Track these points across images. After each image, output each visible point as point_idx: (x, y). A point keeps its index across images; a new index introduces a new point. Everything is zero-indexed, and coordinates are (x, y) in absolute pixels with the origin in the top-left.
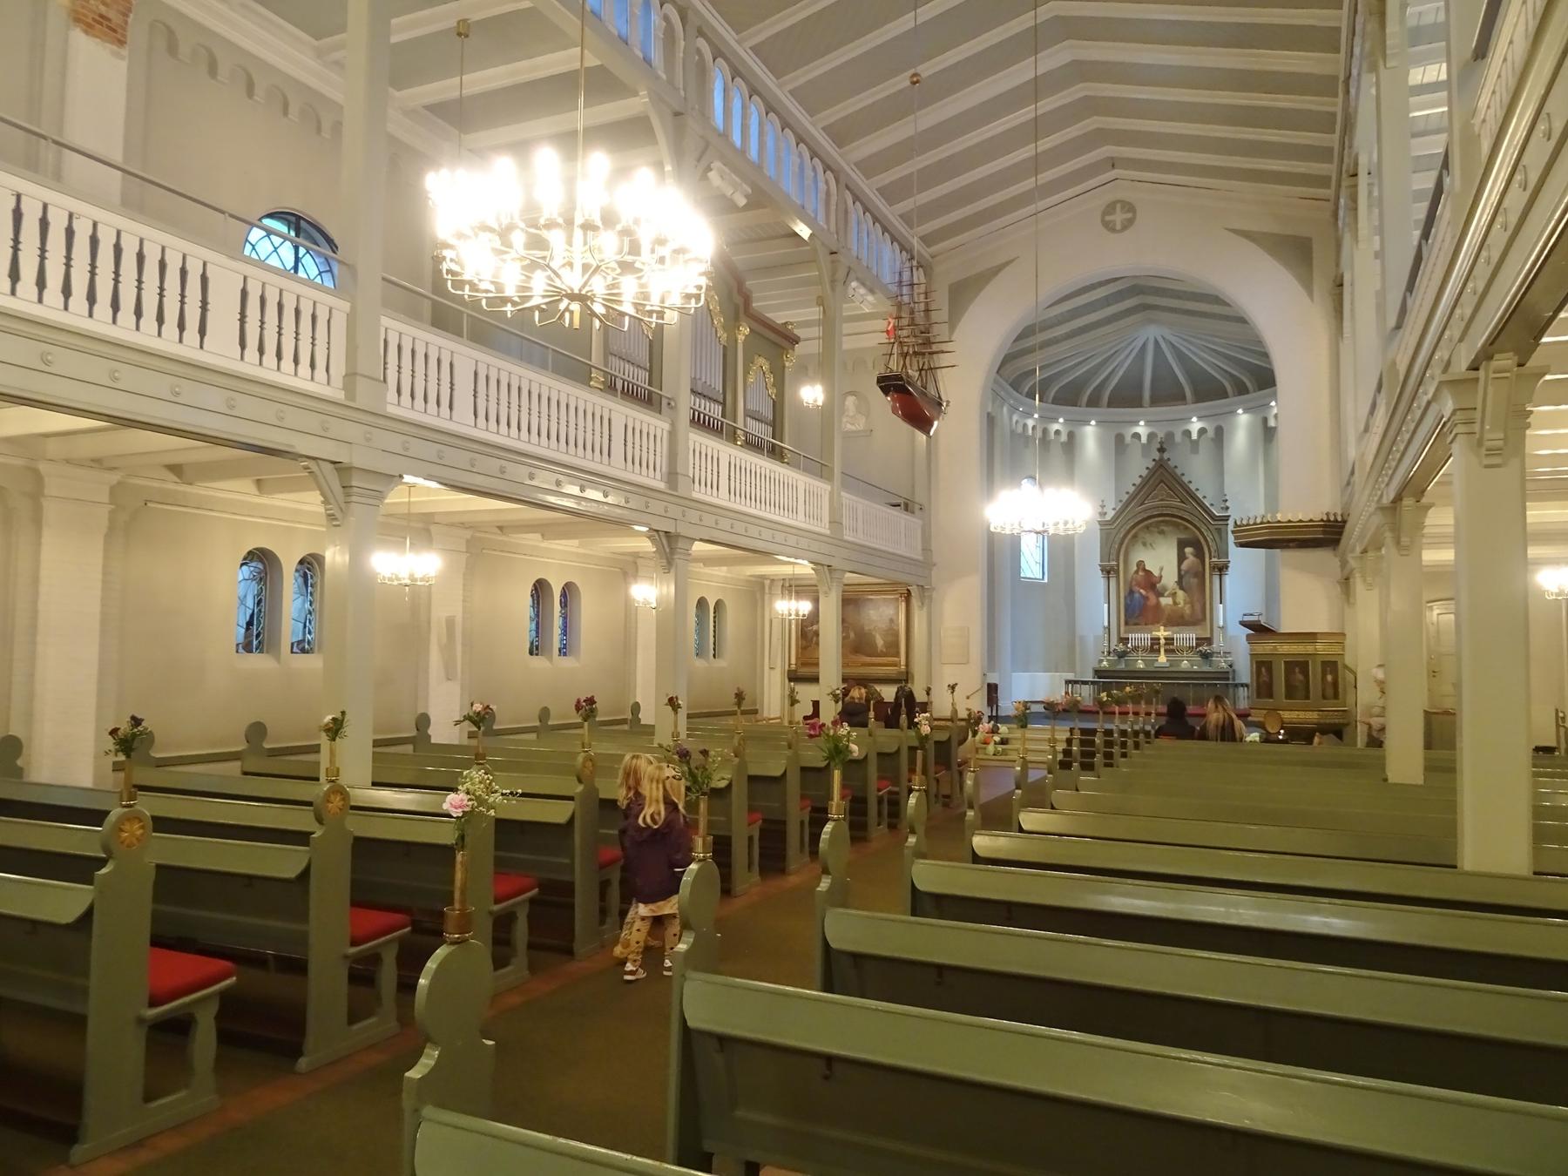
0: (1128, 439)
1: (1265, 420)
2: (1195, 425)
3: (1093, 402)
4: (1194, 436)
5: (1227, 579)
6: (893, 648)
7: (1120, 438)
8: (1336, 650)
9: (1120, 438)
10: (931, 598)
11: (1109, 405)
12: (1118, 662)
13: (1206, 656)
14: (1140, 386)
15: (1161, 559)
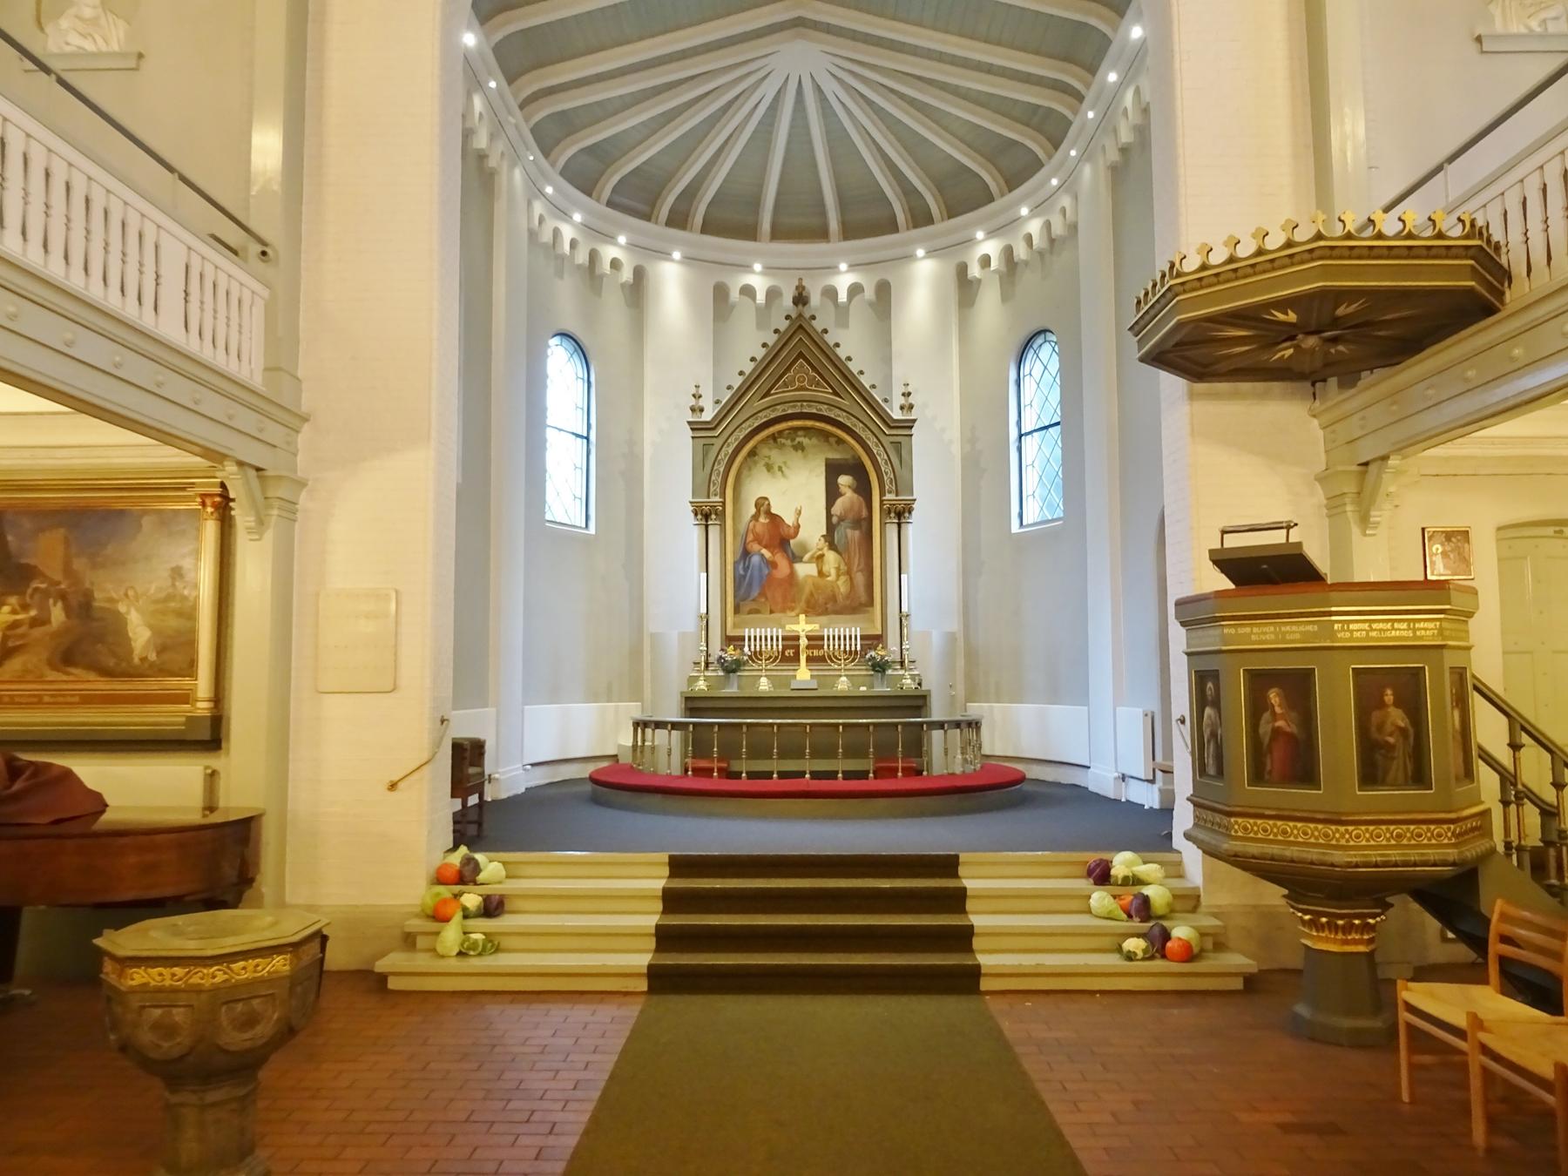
0: (735, 295)
1: (962, 269)
2: (844, 281)
3: (678, 220)
4: (843, 297)
5: (910, 531)
6: (175, 653)
7: (721, 292)
8: (1426, 629)
9: (721, 292)
10: (290, 507)
11: (705, 230)
12: (725, 681)
13: (880, 667)
14: (755, 204)
15: (796, 491)
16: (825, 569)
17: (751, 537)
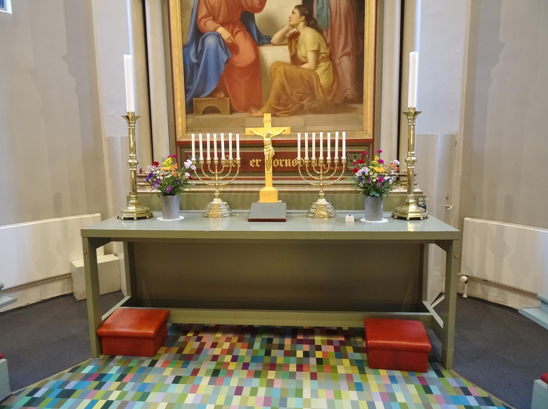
16: (301, 52)
17: (203, 11)
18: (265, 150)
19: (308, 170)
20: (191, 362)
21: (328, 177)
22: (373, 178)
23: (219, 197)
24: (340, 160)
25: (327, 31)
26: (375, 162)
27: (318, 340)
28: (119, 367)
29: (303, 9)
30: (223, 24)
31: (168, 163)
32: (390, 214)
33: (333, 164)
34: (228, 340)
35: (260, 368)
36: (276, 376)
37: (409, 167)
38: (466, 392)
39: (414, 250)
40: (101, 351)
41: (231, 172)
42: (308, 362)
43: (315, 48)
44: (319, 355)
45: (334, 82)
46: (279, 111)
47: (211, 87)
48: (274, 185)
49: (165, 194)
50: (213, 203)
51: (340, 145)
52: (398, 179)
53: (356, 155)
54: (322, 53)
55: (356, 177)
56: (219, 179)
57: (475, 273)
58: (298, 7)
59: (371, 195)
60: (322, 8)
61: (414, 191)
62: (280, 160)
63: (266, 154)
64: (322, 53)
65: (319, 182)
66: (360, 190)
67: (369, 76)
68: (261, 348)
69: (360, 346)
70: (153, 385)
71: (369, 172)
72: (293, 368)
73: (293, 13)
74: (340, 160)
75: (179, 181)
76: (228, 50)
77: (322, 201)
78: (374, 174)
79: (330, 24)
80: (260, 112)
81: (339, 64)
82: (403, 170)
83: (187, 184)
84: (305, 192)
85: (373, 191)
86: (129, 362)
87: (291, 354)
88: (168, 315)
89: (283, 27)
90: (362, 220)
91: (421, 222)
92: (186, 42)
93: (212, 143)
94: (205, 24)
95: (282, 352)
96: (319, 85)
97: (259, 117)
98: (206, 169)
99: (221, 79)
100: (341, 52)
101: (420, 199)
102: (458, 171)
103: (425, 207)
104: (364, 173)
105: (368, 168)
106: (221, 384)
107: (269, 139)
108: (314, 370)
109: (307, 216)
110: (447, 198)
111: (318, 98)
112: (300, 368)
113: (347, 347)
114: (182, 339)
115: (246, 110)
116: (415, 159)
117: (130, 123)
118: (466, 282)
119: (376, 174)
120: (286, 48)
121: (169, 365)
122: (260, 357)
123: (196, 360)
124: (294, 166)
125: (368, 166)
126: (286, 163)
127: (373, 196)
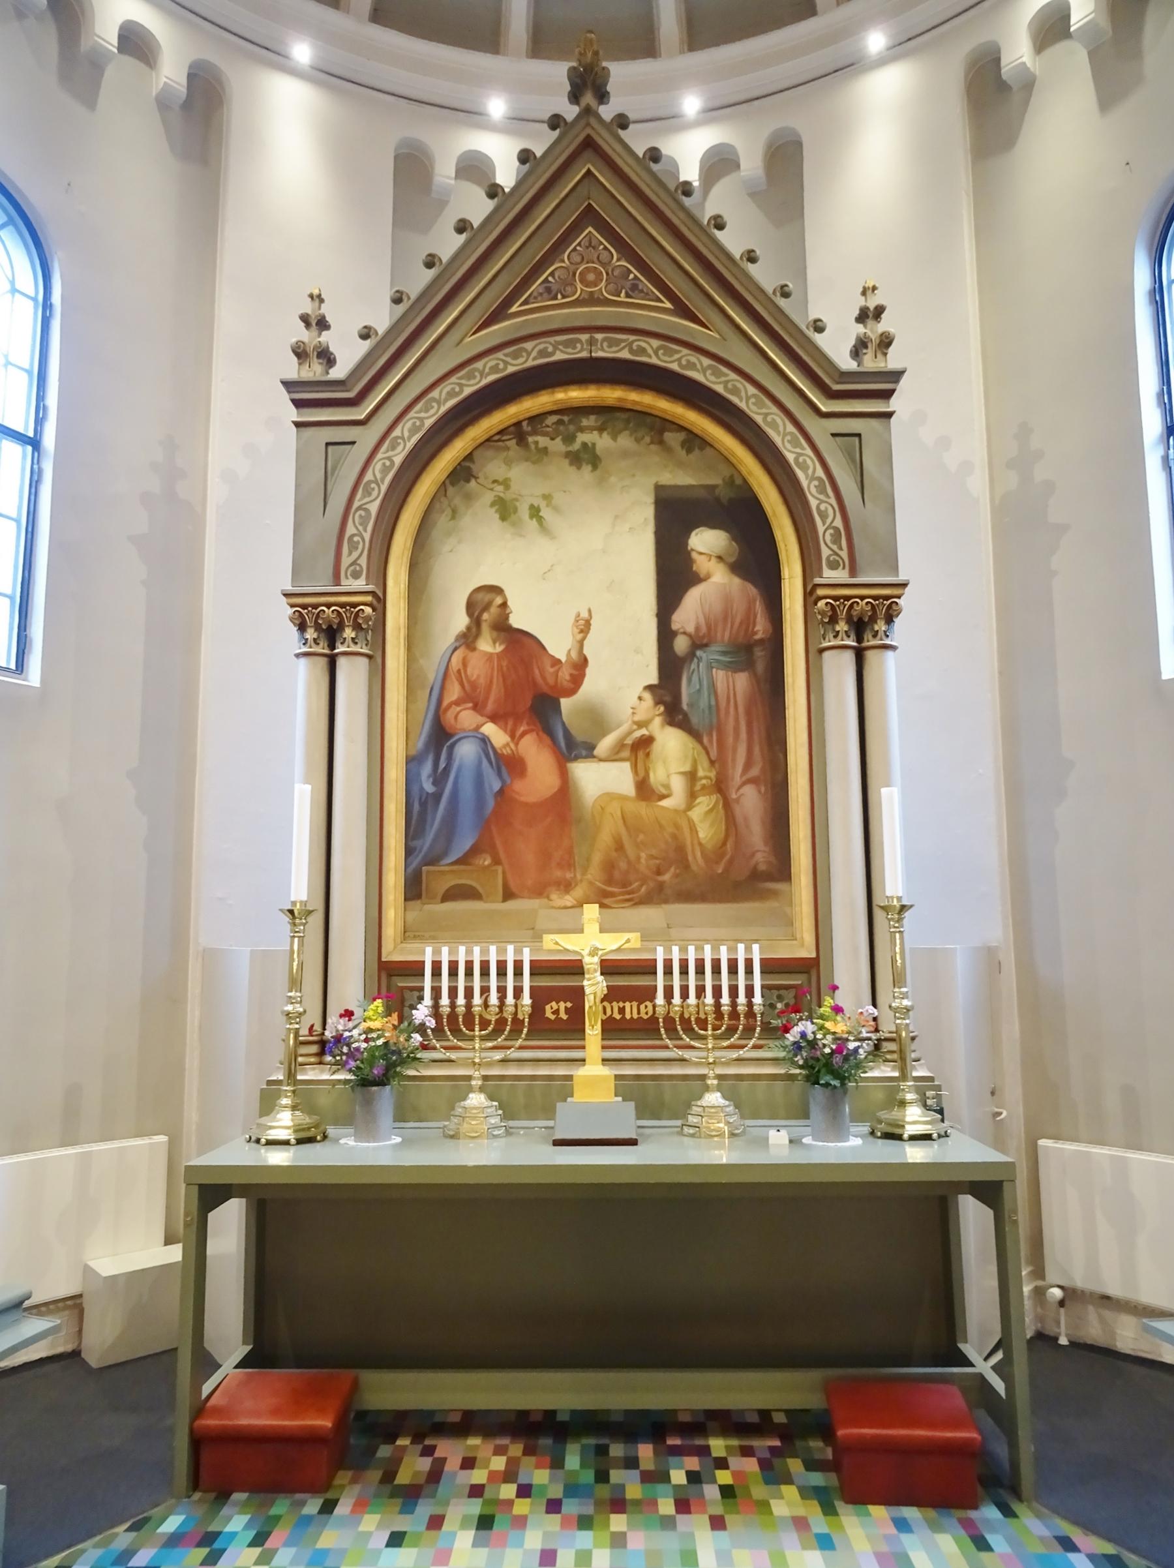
15: (578, 571)
16: (657, 776)
17: (454, 692)
18: (585, 983)
19: (684, 1027)
20: (420, 1501)
21: (725, 1044)
22: (824, 1046)
23: (481, 1089)
24: (750, 1005)
25: (710, 735)
26: (825, 1010)
27: (718, 1445)
28: (249, 1516)
29: (662, 691)
30: (494, 718)
31: (376, 1011)
32: (865, 1129)
33: (734, 1014)
34: (499, 1451)
35: (589, 1510)
36: (628, 1524)
37: (898, 1021)
38: (1068, 1545)
39: (927, 1205)
40: (195, 1483)
41: (511, 1031)
42: (702, 1495)
43: (687, 768)
44: (724, 1477)
45: (727, 830)
46: (612, 895)
47: (464, 843)
48: (605, 1061)
49: (365, 1082)
50: (468, 1103)
51: (749, 971)
52: (877, 1047)
53: (782, 992)
54: (701, 778)
55: (787, 1043)
56: (481, 1049)
57: (1080, 1281)
58: (649, 688)
59: (822, 1082)
60: (699, 691)
61: (915, 1074)
62: (614, 1004)
63: (588, 991)
64: (701, 778)
65: (704, 1054)
66: (798, 1071)
67: (801, 825)
68: (583, 1465)
69: (817, 1456)
70: (342, 1553)
71: (813, 1033)
72: (667, 1507)
73: (640, 698)
74: (750, 1005)
75: (399, 1053)
76: (504, 770)
77: (714, 1098)
78: (824, 1036)
79: (715, 720)
80: (568, 897)
81: (737, 801)
82: (887, 1027)
83: (415, 1059)
84: (671, 1077)
85: (826, 1074)
86: (272, 1504)
87: (658, 1477)
88: (355, 1386)
89: (619, 726)
90: (805, 1140)
91: (935, 1145)
92: (413, 752)
93: (469, 966)
94: (456, 717)
95: (635, 1474)
96: (696, 842)
97: (566, 908)
98: (454, 1025)
99: (485, 826)
100: (741, 776)
101: (930, 1093)
102: (1012, 1029)
103: (941, 1112)
104: (803, 1035)
105: (813, 1023)
106: (502, 1543)
107: (596, 959)
108: (718, 1510)
109: (681, 1133)
110: (993, 1093)
111: (694, 867)
112: (683, 1506)
113: (789, 1460)
114: (384, 1451)
115: (540, 891)
116: (909, 1004)
117: (294, 924)
118: (1062, 1303)
119: (829, 1037)
120: (626, 766)
121: (369, 1508)
122: (586, 1485)
123: (433, 1495)
124: (645, 1017)
125: (810, 1018)
126: (628, 1010)
127: (827, 1085)
